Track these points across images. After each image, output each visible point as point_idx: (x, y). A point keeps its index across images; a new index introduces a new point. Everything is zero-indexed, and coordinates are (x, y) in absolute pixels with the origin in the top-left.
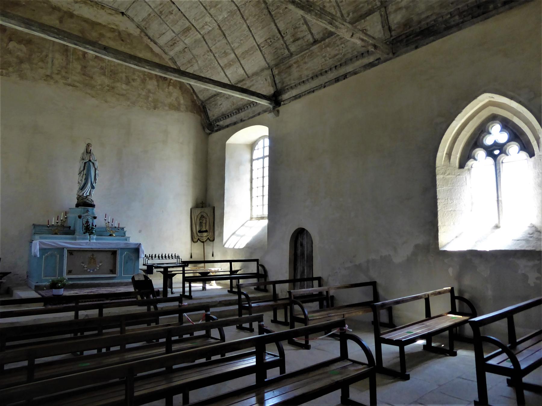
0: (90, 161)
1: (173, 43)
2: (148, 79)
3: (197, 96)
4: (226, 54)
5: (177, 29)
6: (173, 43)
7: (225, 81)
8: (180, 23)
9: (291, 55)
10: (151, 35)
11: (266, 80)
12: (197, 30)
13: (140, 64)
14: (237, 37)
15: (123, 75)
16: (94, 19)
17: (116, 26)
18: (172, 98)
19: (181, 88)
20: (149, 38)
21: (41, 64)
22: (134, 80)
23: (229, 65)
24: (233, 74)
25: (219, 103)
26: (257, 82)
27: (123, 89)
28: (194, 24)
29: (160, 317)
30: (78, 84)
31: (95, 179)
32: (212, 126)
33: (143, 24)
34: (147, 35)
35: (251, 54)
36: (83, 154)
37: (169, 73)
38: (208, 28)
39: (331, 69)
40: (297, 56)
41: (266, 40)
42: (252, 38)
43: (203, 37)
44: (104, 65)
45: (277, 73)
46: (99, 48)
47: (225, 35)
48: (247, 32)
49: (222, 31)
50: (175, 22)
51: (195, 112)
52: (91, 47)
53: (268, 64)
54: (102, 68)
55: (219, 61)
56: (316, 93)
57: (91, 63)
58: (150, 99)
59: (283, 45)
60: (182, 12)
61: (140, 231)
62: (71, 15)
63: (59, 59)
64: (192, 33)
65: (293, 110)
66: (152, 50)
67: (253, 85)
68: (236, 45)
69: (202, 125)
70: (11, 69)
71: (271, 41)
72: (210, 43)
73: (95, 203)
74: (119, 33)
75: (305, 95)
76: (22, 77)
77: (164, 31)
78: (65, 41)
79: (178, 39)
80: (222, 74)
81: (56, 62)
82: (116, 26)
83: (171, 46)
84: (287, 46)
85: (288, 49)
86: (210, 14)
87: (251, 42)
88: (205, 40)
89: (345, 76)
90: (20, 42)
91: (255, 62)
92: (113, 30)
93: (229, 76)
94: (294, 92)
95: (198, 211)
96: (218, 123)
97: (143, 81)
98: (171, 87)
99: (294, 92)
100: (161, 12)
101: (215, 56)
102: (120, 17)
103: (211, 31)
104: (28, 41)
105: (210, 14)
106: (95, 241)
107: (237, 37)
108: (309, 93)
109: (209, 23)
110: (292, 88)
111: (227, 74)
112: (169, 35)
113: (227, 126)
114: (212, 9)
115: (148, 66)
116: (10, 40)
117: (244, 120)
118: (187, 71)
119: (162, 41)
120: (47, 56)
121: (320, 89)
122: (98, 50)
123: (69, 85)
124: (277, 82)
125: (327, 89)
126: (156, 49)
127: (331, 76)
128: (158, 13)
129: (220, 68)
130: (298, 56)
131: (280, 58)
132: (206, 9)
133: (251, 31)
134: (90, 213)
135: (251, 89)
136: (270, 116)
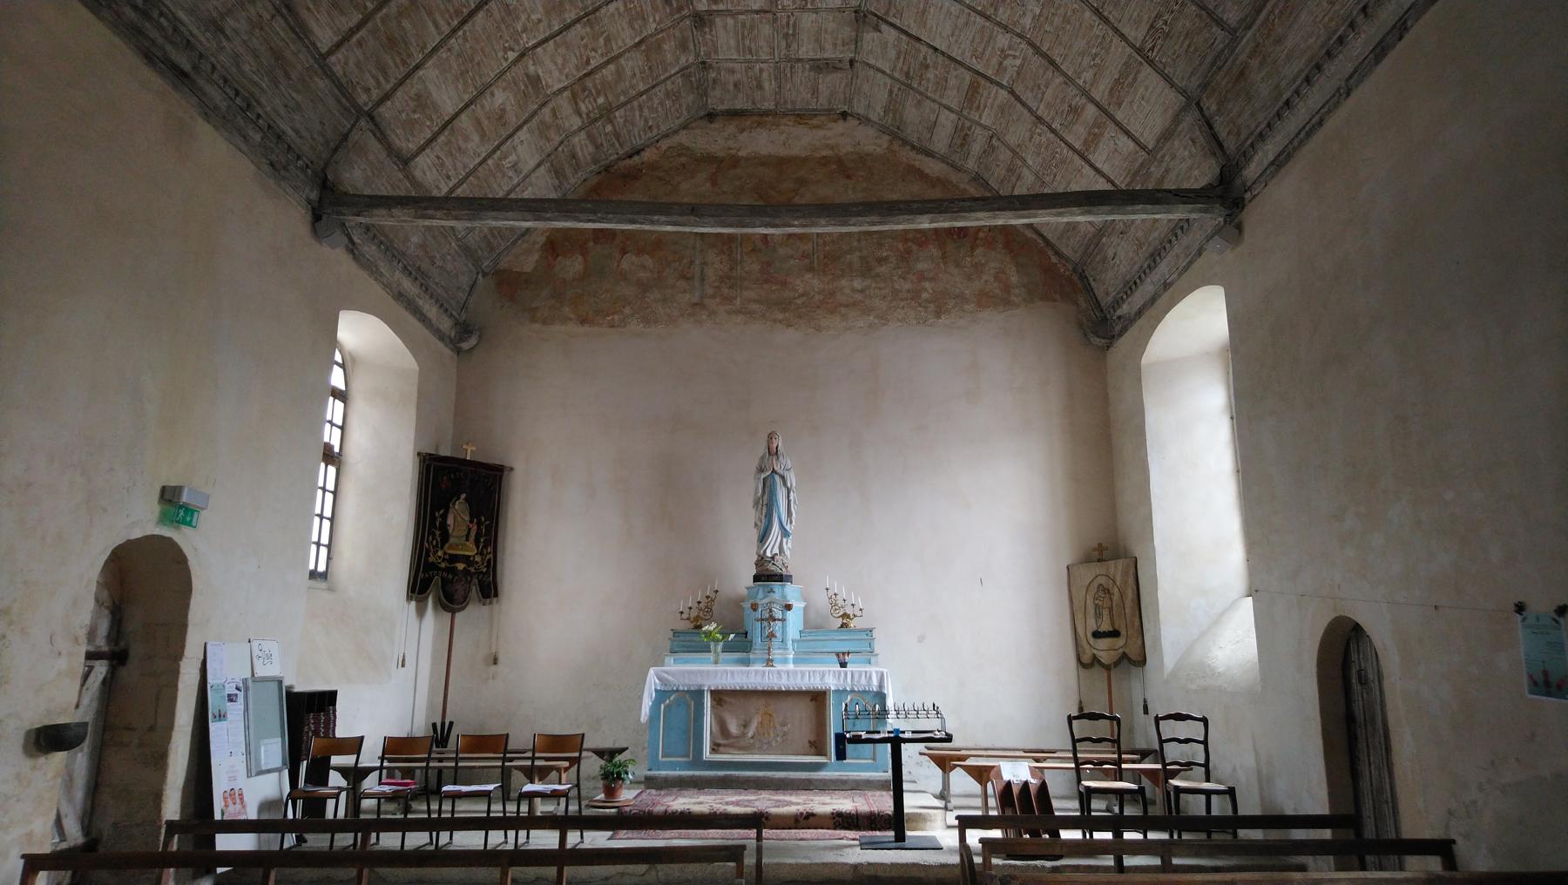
0: (774, 471)
1: (962, 137)
2: (915, 247)
3: (1057, 253)
4: (1075, 111)
5: (953, 98)
6: (962, 137)
7: (1102, 185)
8: (952, 82)
9: (1234, 34)
10: (914, 139)
11: (1194, 142)
12: (992, 81)
13: (777, 221)
14: (1082, 54)
15: (854, 258)
16: (783, 152)
17: (832, 148)
18: (985, 277)
19: (1008, 245)
20: (913, 147)
21: (682, 284)
22: (881, 261)
23: (1093, 139)
24: (1113, 161)
25: (1110, 253)
26: (1173, 157)
27: (854, 290)
28: (979, 67)
29: (218, 816)
30: (754, 307)
31: (789, 513)
32: (1099, 324)
33: (889, 119)
34: (905, 142)
35: (1131, 85)
36: (762, 458)
37: (853, 220)
38: (1012, 64)
39: (1352, 25)
40: (1249, 34)
41: (1152, 26)
42: (1116, 40)
43: (1012, 92)
44: (808, 247)
45: (1214, 108)
46: (681, 215)
47: (1052, 62)
48: (1099, 29)
49: (1045, 56)
50: (942, 83)
51: (1057, 296)
52: (663, 218)
53: (1183, 92)
54: (804, 256)
55: (1069, 139)
56: (1330, 124)
57: (782, 251)
58: (925, 295)
59: (1199, 16)
60: (943, 53)
61: (921, 639)
62: (735, 162)
63: (716, 264)
64: (985, 93)
65: (1279, 202)
66: (922, 175)
67: (1167, 171)
68: (1088, 76)
69: (1081, 326)
70: (627, 311)
71: (1165, 23)
72: (1028, 97)
73: (791, 571)
74: (839, 161)
75: (1301, 143)
76: (647, 321)
77: (933, 118)
78: (610, 221)
79: (967, 124)
80: (1087, 170)
81: (709, 272)
82: (832, 148)
83: (962, 145)
84: (1210, 14)
85: (1220, 23)
86: (999, 24)
87: (1119, 53)
88: (1018, 98)
89: (1401, 28)
90: (640, 252)
91: (1150, 107)
92: (824, 162)
93: (1106, 169)
94: (1270, 150)
95: (1088, 573)
96: (1119, 312)
97: (905, 256)
98: (979, 251)
99: (1270, 150)
100: (907, 75)
101: (1053, 131)
102: (840, 127)
103: (1022, 65)
104: (657, 244)
105: (999, 24)
106: (791, 666)
107: (1082, 54)
108: (1308, 135)
109: (1010, 48)
110: (1261, 136)
111: (1099, 165)
112: (947, 121)
113: (1140, 313)
114: (1001, 10)
115: (797, 218)
116: (624, 252)
117: (1171, 284)
118: (1016, 193)
119: (941, 142)
120: (692, 262)
121: (1337, 105)
122: (679, 219)
123: (738, 312)
124: (1223, 135)
125: (1355, 95)
126: (934, 168)
127: (1359, 46)
128: (903, 79)
129: (1076, 157)
130: (1255, 27)
131: (1209, 59)
132: (988, 18)
133: (1106, 20)
134: (777, 596)
135: (1169, 185)
136: (1215, 253)
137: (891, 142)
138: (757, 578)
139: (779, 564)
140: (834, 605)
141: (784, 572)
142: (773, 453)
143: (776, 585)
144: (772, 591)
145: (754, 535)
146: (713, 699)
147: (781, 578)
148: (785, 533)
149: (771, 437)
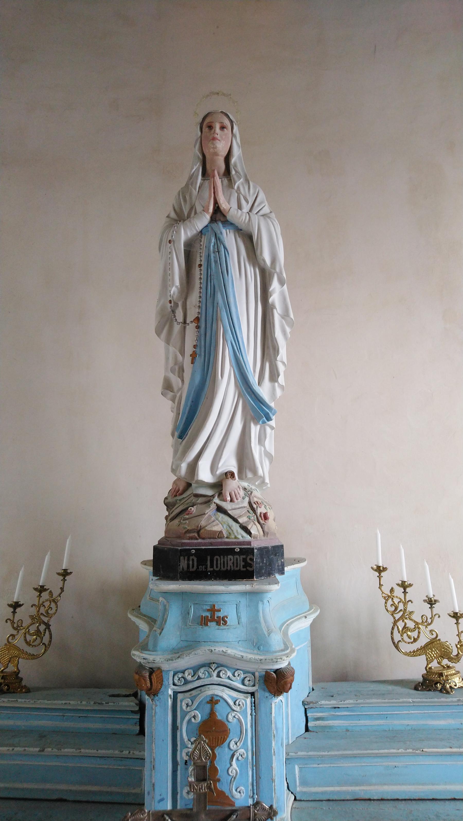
0: (218, 215)
73: (278, 530)
134: (230, 642)
137: (441, 662)
138: (168, 561)
139: (238, 508)
140: (399, 613)
141: (258, 539)
142: (213, 169)
143: (228, 594)
144: (214, 617)
145: (165, 414)
146: (208, 209)
147: (247, 564)
148: (256, 409)
149: (207, 125)
